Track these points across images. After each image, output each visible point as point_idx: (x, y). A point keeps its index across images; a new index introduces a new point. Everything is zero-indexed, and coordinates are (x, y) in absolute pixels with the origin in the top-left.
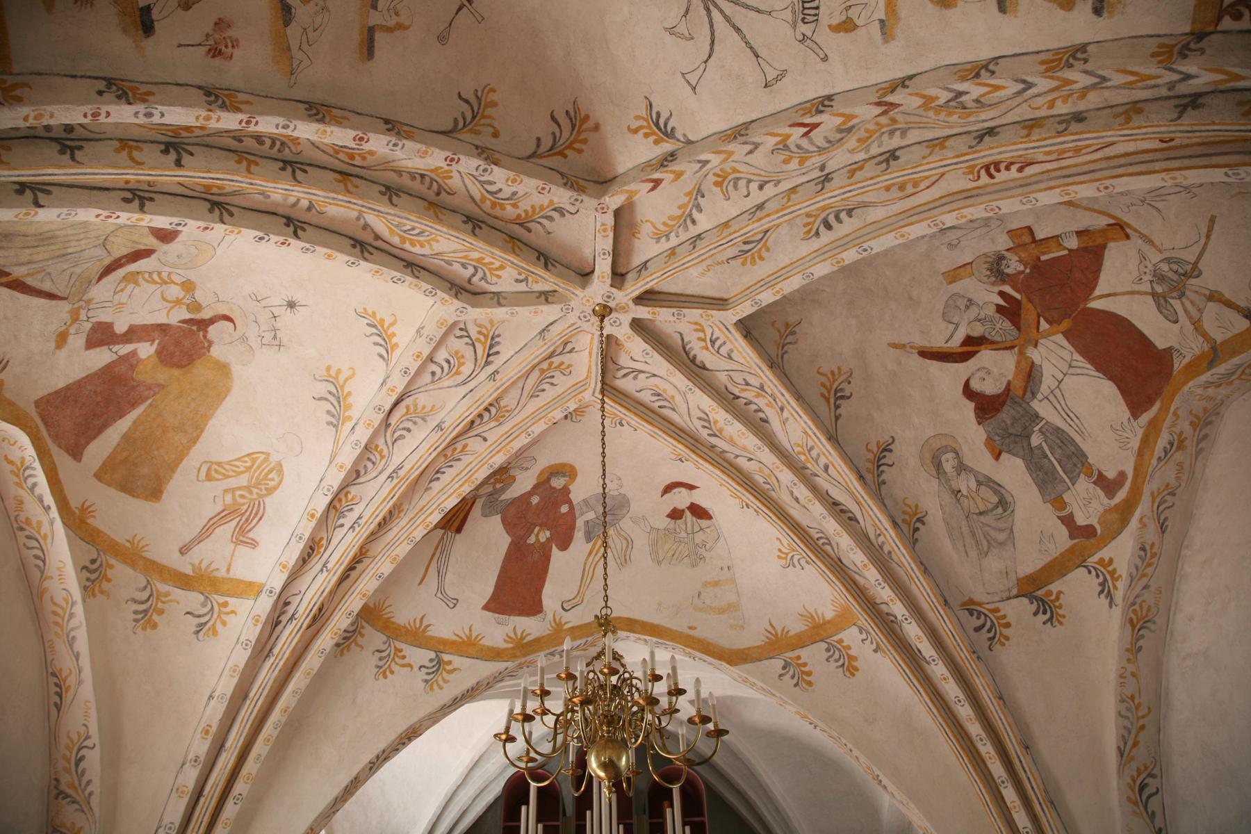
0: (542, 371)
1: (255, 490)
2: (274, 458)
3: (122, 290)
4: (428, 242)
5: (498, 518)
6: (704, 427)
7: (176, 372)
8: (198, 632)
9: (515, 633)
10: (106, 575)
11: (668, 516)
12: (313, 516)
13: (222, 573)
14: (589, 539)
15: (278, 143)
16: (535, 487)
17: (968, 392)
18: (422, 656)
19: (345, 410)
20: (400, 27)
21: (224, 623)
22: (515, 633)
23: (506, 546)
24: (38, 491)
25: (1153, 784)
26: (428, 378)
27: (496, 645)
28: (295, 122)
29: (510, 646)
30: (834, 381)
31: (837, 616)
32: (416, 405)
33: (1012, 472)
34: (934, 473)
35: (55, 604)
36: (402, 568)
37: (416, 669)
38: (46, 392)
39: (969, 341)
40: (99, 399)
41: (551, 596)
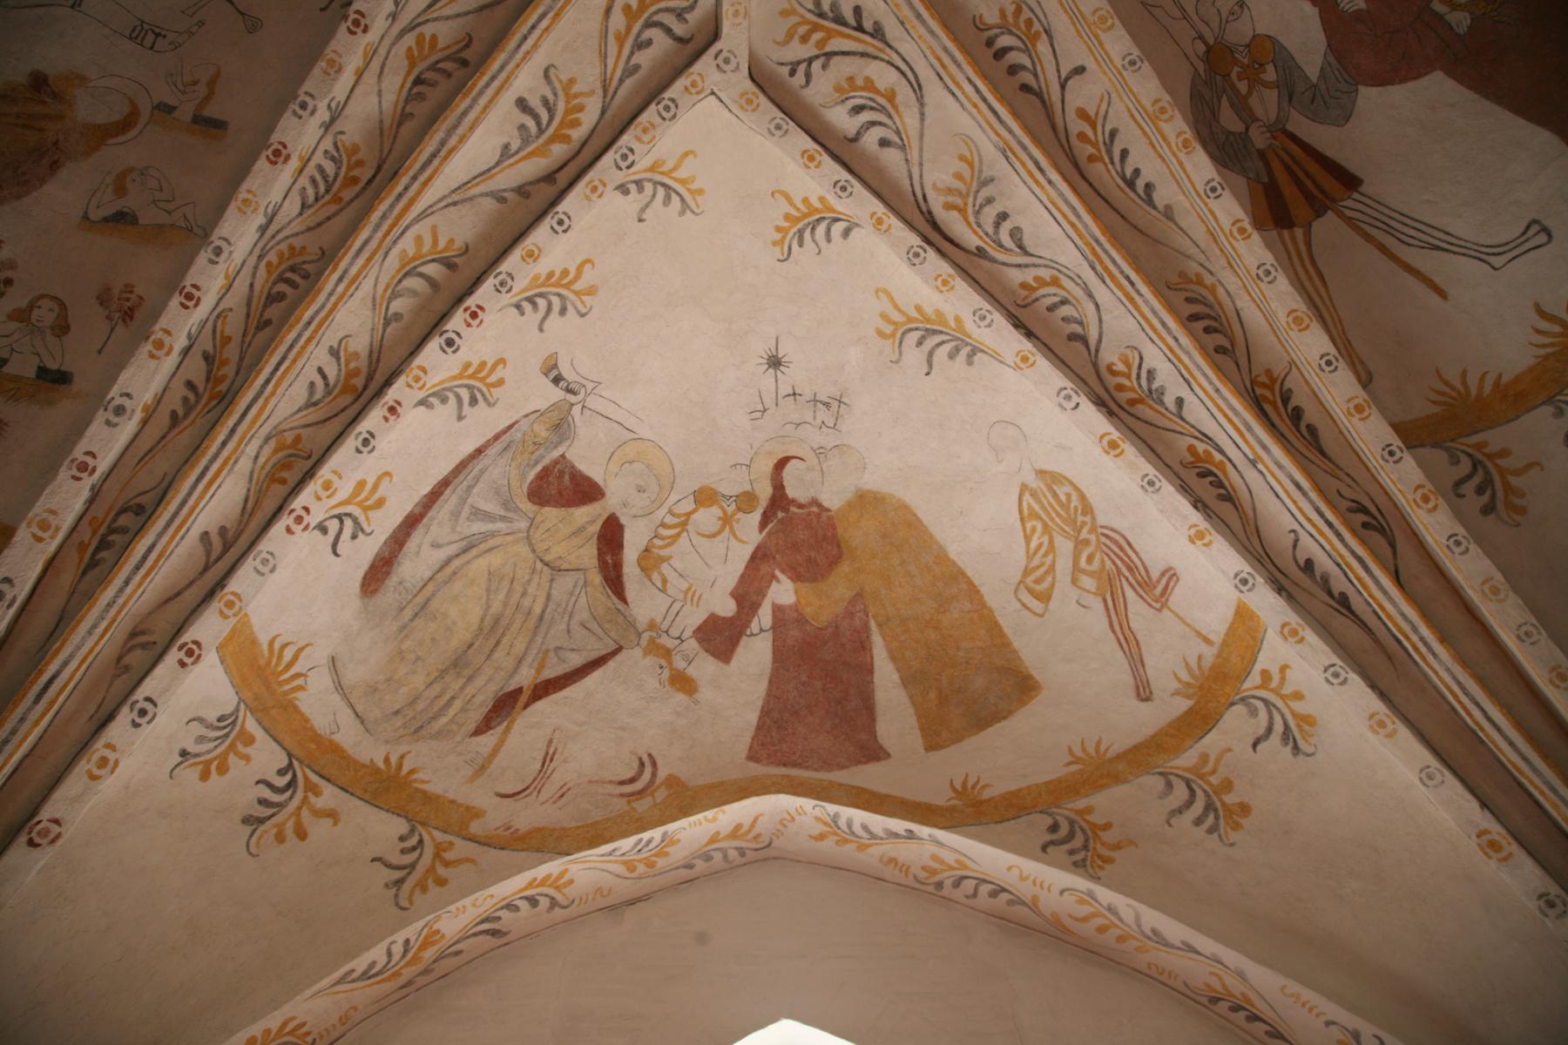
1: (1084, 534)
3: (665, 581)
4: (569, 97)
7: (845, 567)
8: (1296, 748)
10: (1094, 826)
12: (1113, 445)
13: (1209, 653)
15: (289, 275)
19: (946, 324)
20: (212, 83)
21: (1298, 696)
24: (878, 831)
26: (891, 157)
28: (214, 237)
32: (949, 191)
35: (1085, 919)
38: (748, 740)
40: (818, 684)
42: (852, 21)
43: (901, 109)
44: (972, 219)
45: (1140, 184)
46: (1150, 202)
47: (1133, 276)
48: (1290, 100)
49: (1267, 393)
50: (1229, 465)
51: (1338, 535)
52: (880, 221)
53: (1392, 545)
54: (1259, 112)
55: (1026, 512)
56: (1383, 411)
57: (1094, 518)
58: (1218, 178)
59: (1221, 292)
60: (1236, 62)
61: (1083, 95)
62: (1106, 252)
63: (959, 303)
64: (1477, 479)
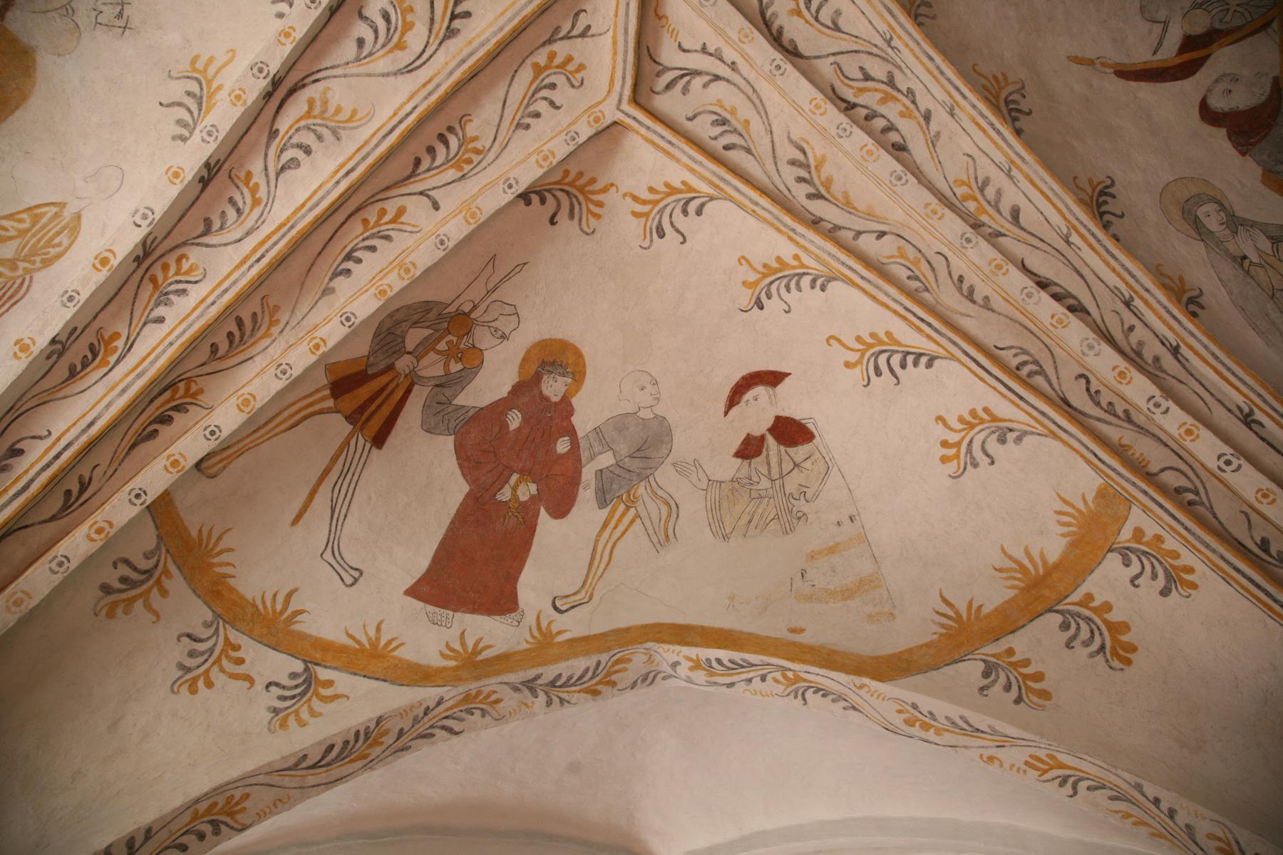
0: (538, 70)
1: (22, 265)
5: (449, 442)
6: (800, 180)
9: (463, 644)
11: (738, 454)
12: (104, 262)
14: (602, 503)
16: (517, 390)
17: (1208, 115)
18: (281, 666)
22: (463, 644)
23: (461, 497)
27: (423, 662)
29: (452, 663)
30: (1001, 88)
31: (1073, 545)
32: (325, 103)
34: (1193, 233)
36: (263, 425)
37: (259, 686)
39: (1189, 43)
41: (533, 587)
42: (459, 10)
43: (391, 55)
44: (302, 123)
45: (349, 265)
46: (336, 274)
47: (265, 261)
48: (437, 386)
49: (181, 392)
50: (105, 370)
51: (48, 465)
52: (287, 35)
53: (53, 518)
54: (424, 362)
55: (38, 211)
56: (176, 484)
57: (39, 269)
58: (358, 321)
59: (267, 341)
60: (460, 338)
61: (417, 210)
62: (283, 236)
63: (224, 116)
64: (134, 576)
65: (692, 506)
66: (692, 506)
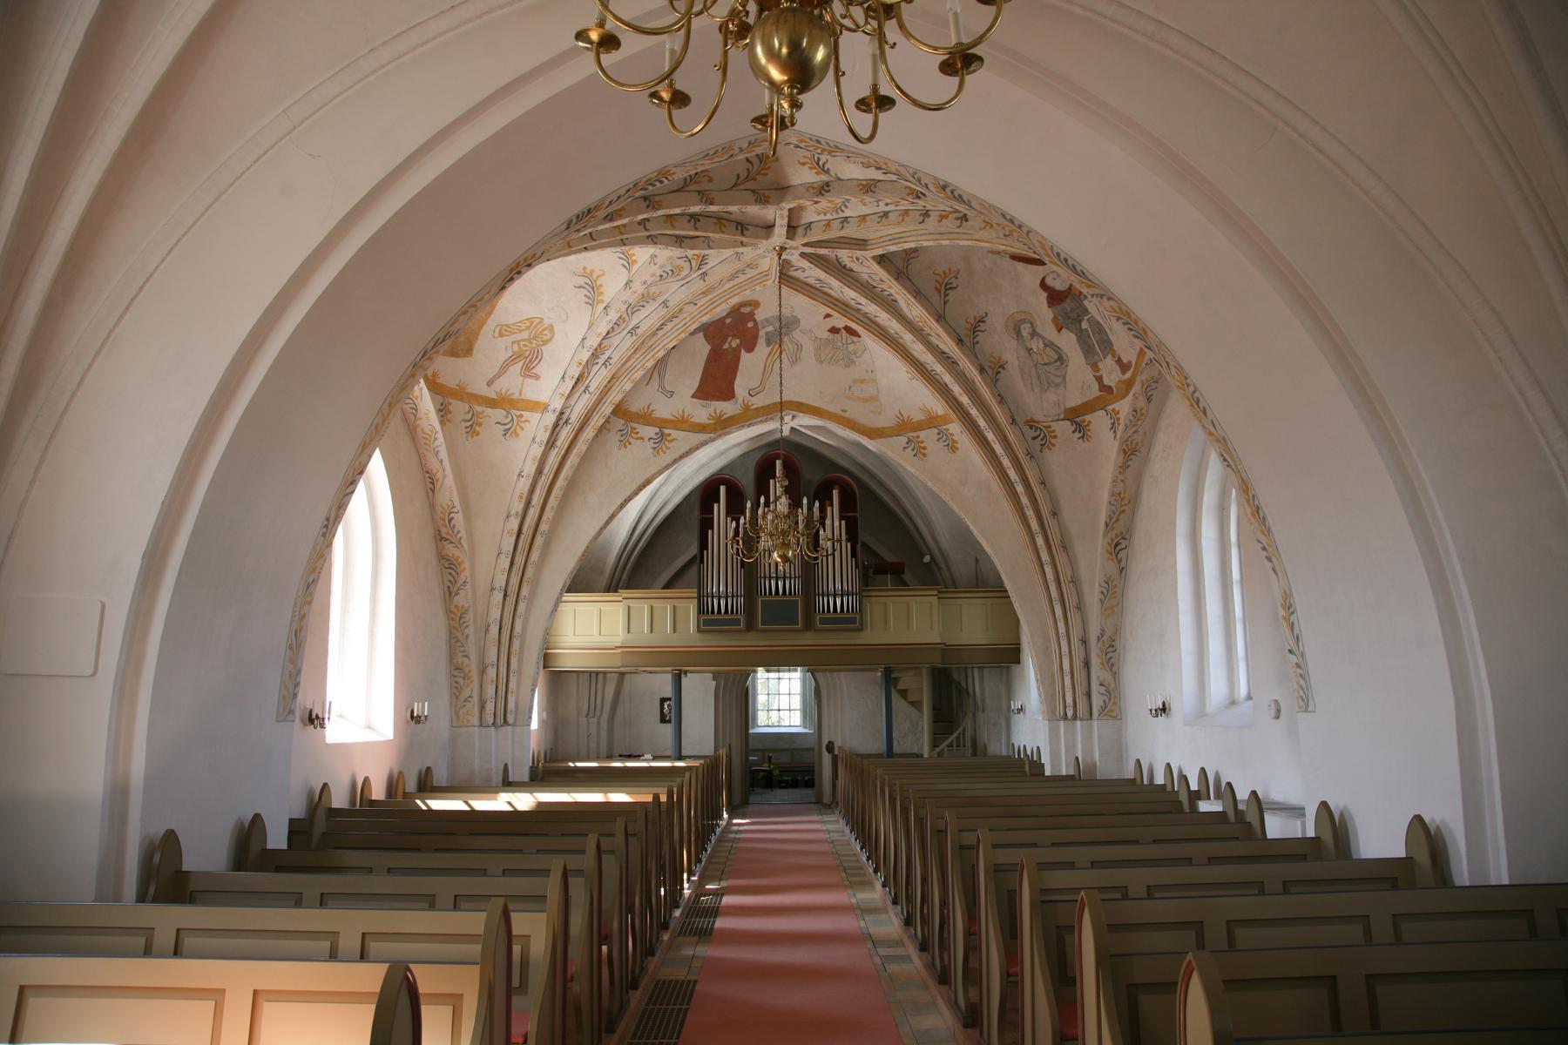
2: (547, 322)
13: (517, 396)
14: (768, 344)
17: (1043, 285)
18: (651, 431)
25: (1124, 543)
33: (1068, 342)
41: (741, 386)
65: (808, 347)
66: (808, 347)
